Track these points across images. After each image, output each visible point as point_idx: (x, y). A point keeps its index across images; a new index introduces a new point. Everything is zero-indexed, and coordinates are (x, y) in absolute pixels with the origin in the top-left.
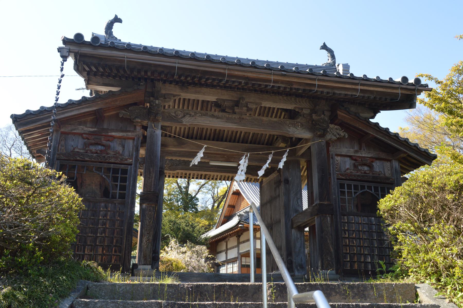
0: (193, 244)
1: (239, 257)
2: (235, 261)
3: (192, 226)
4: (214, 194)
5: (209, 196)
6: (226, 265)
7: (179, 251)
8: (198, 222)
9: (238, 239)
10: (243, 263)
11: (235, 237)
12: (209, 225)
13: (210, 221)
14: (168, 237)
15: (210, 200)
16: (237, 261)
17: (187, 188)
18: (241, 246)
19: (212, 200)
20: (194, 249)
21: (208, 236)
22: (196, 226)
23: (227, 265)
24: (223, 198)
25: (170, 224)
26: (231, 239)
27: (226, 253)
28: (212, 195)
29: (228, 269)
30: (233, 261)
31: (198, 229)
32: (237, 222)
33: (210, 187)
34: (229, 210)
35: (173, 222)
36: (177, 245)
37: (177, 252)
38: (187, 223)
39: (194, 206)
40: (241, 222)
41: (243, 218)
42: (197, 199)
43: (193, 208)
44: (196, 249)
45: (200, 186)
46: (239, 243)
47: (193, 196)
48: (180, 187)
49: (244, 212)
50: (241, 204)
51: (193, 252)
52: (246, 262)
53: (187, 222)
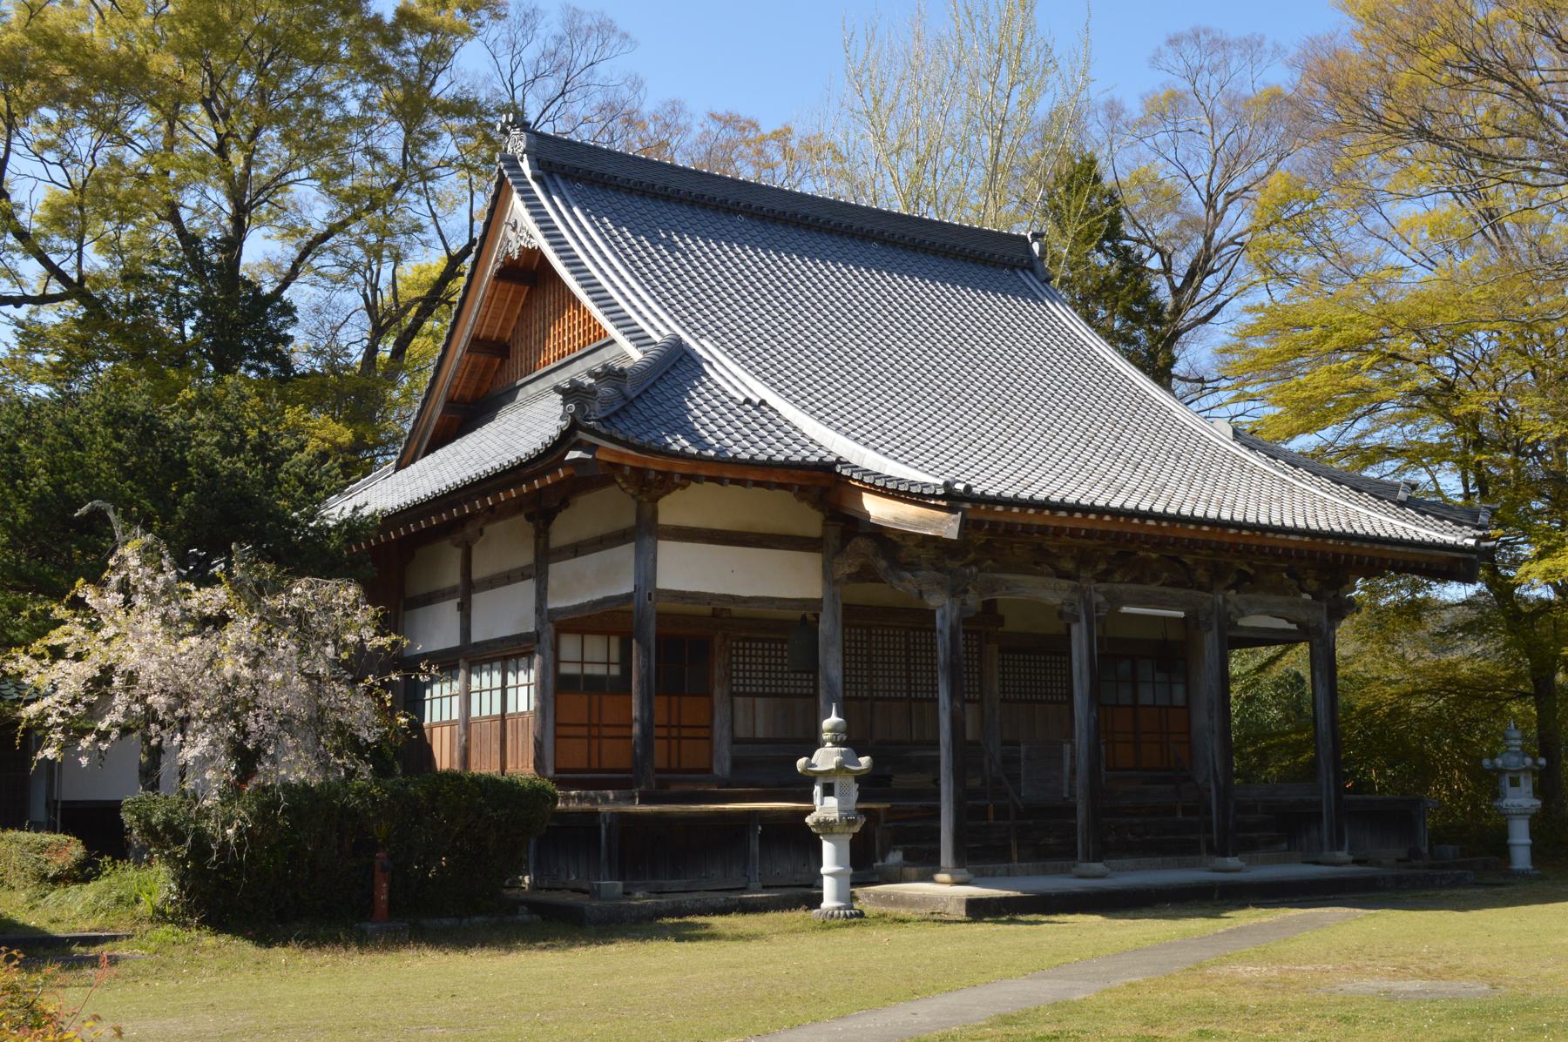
0: (268, 569)
1: (548, 636)
2: (518, 656)
3: (259, 449)
4: (375, 288)
5: (352, 299)
6: (462, 673)
7: (176, 613)
8: (294, 431)
9: (542, 534)
10: (566, 669)
11: (521, 518)
12: (358, 446)
13: (360, 428)
14: (98, 516)
15: (354, 319)
16: (529, 654)
17: (233, 244)
18: (559, 571)
19: (367, 323)
20: (278, 602)
21: (366, 512)
22: (291, 452)
23: (469, 673)
24: (426, 310)
25: (119, 438)
26: (496, 529)
27: (465, 610)
28: (365, 296)
29: (475, 698)
30: (505, 653)
31: (301, 470)
32: (555, 433)
33: (357, 253)
34: (475, 366)
35: (135, 421)
36: (160, 570)
37: (163, 617)
38: (228, 434)
39: (273, 346)
40: (581, 435)
41: (596, 410)
42: (288, 310)
43: (264, 355)
44: (293, 603)
45: (304, 245)
46: (545, 556)
47: (267, 289)
48: (190, 240)
49: (591, 374)
50: (546, 336)
51: (274, 621)
52: (582, 662)
53: (228, 425)
